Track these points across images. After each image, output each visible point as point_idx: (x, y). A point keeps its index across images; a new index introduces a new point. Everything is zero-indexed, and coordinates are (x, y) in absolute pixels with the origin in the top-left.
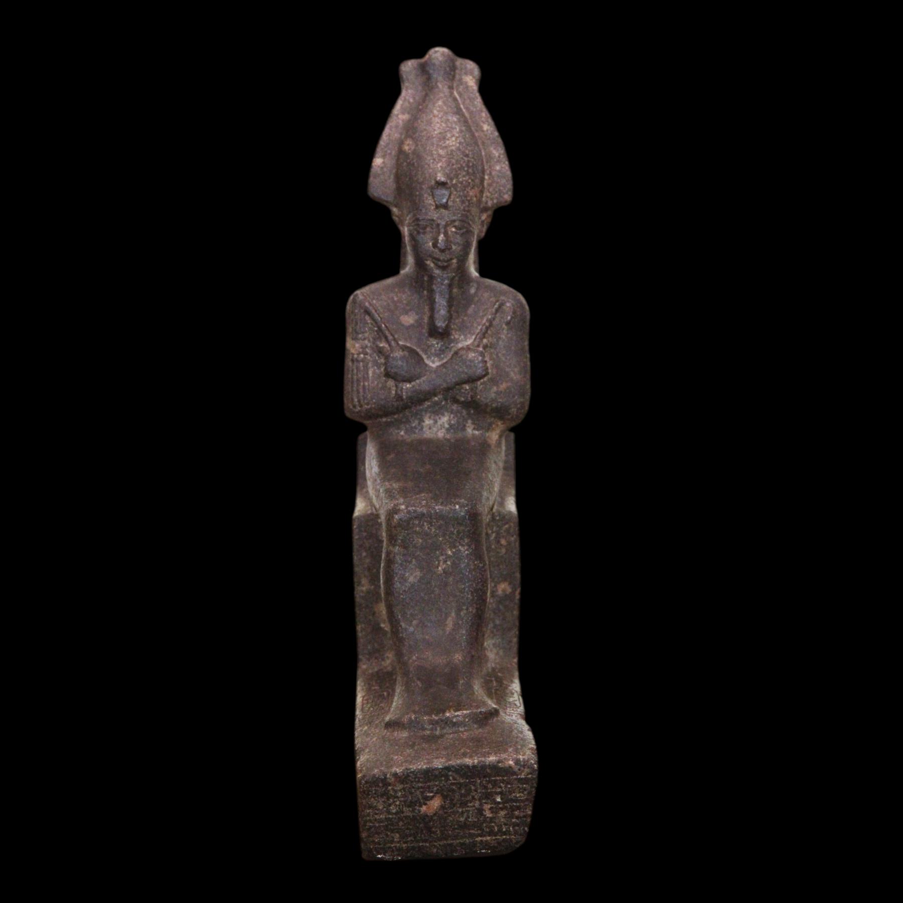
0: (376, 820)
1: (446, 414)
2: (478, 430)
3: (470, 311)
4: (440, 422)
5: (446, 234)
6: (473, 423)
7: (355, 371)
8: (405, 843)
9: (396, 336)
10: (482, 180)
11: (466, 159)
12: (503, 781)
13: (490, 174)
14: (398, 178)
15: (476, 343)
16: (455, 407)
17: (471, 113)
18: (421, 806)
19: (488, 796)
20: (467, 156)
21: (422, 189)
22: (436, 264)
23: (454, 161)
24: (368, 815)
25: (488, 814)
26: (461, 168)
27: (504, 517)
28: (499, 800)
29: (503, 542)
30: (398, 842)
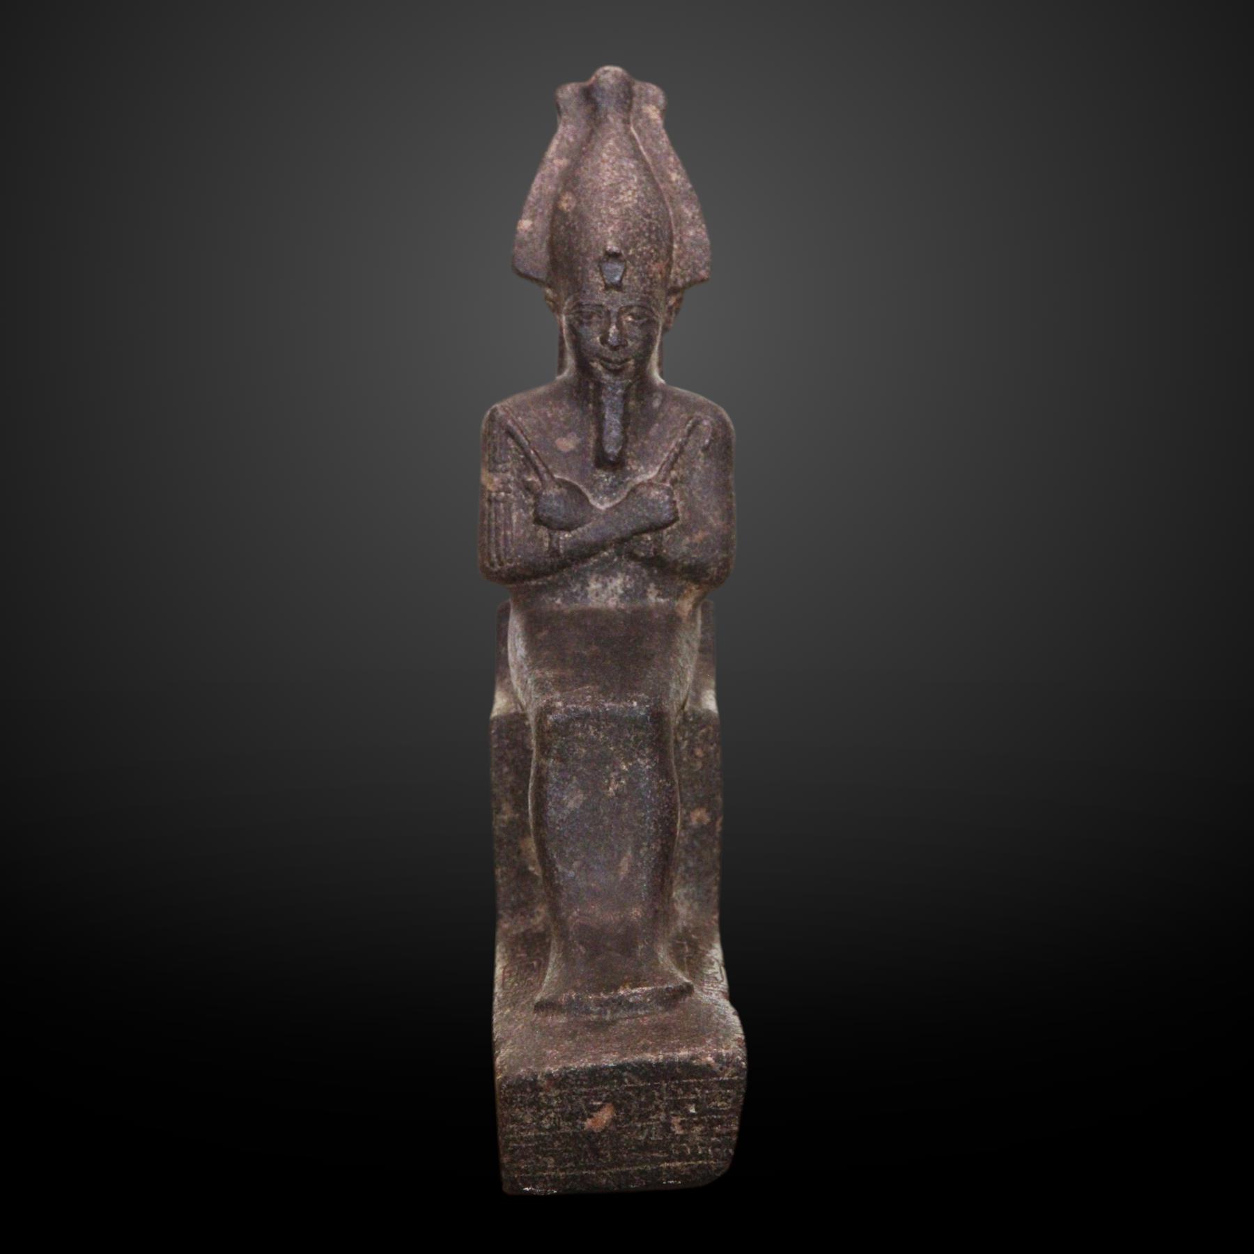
0: (522, 1138)
1: (619, 575)
2: (663, 597)
3: (653, 432)
4: (610, 587)
5: (619, 325)
6: (657, 588)
7: (493, 516)
8: (562, 1170)
9: (550, 467)
10: (670, 250)
11: (647, 221)
12: (698, 1085)
13: (681, 242)
14: (552, 247)
15: (661, 477)
16: (632, 565)
17: (654, 157)
18: (584, 1119)
19: (678, 1106)
20: (649, 216)
21: (585, 262)
22: (605, 367)
23: (630, 224)
24: (512, 1131)
25: (678, 1131)
26: (641, 233)
27: (700, 718)
28: (693, 1111)
29: (699, 752)
30: (553, 1170)
